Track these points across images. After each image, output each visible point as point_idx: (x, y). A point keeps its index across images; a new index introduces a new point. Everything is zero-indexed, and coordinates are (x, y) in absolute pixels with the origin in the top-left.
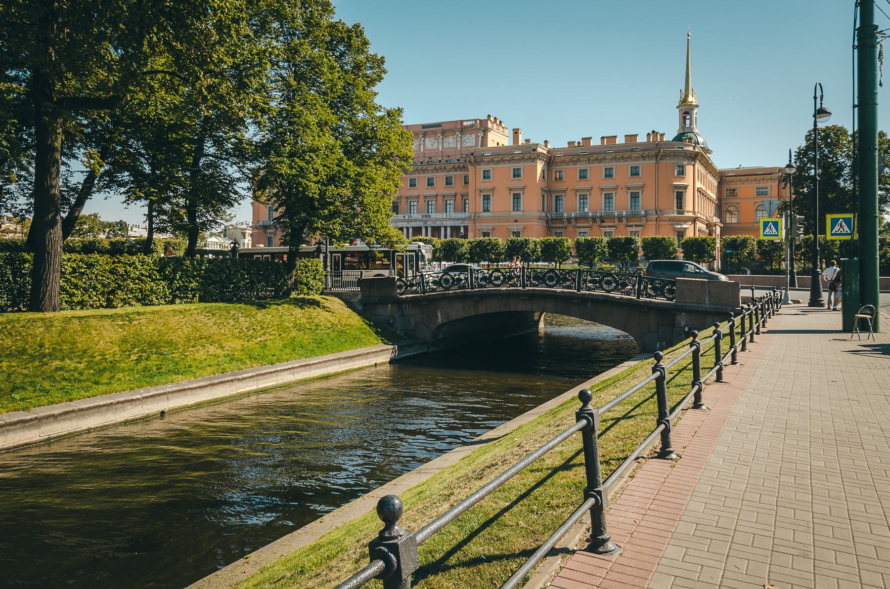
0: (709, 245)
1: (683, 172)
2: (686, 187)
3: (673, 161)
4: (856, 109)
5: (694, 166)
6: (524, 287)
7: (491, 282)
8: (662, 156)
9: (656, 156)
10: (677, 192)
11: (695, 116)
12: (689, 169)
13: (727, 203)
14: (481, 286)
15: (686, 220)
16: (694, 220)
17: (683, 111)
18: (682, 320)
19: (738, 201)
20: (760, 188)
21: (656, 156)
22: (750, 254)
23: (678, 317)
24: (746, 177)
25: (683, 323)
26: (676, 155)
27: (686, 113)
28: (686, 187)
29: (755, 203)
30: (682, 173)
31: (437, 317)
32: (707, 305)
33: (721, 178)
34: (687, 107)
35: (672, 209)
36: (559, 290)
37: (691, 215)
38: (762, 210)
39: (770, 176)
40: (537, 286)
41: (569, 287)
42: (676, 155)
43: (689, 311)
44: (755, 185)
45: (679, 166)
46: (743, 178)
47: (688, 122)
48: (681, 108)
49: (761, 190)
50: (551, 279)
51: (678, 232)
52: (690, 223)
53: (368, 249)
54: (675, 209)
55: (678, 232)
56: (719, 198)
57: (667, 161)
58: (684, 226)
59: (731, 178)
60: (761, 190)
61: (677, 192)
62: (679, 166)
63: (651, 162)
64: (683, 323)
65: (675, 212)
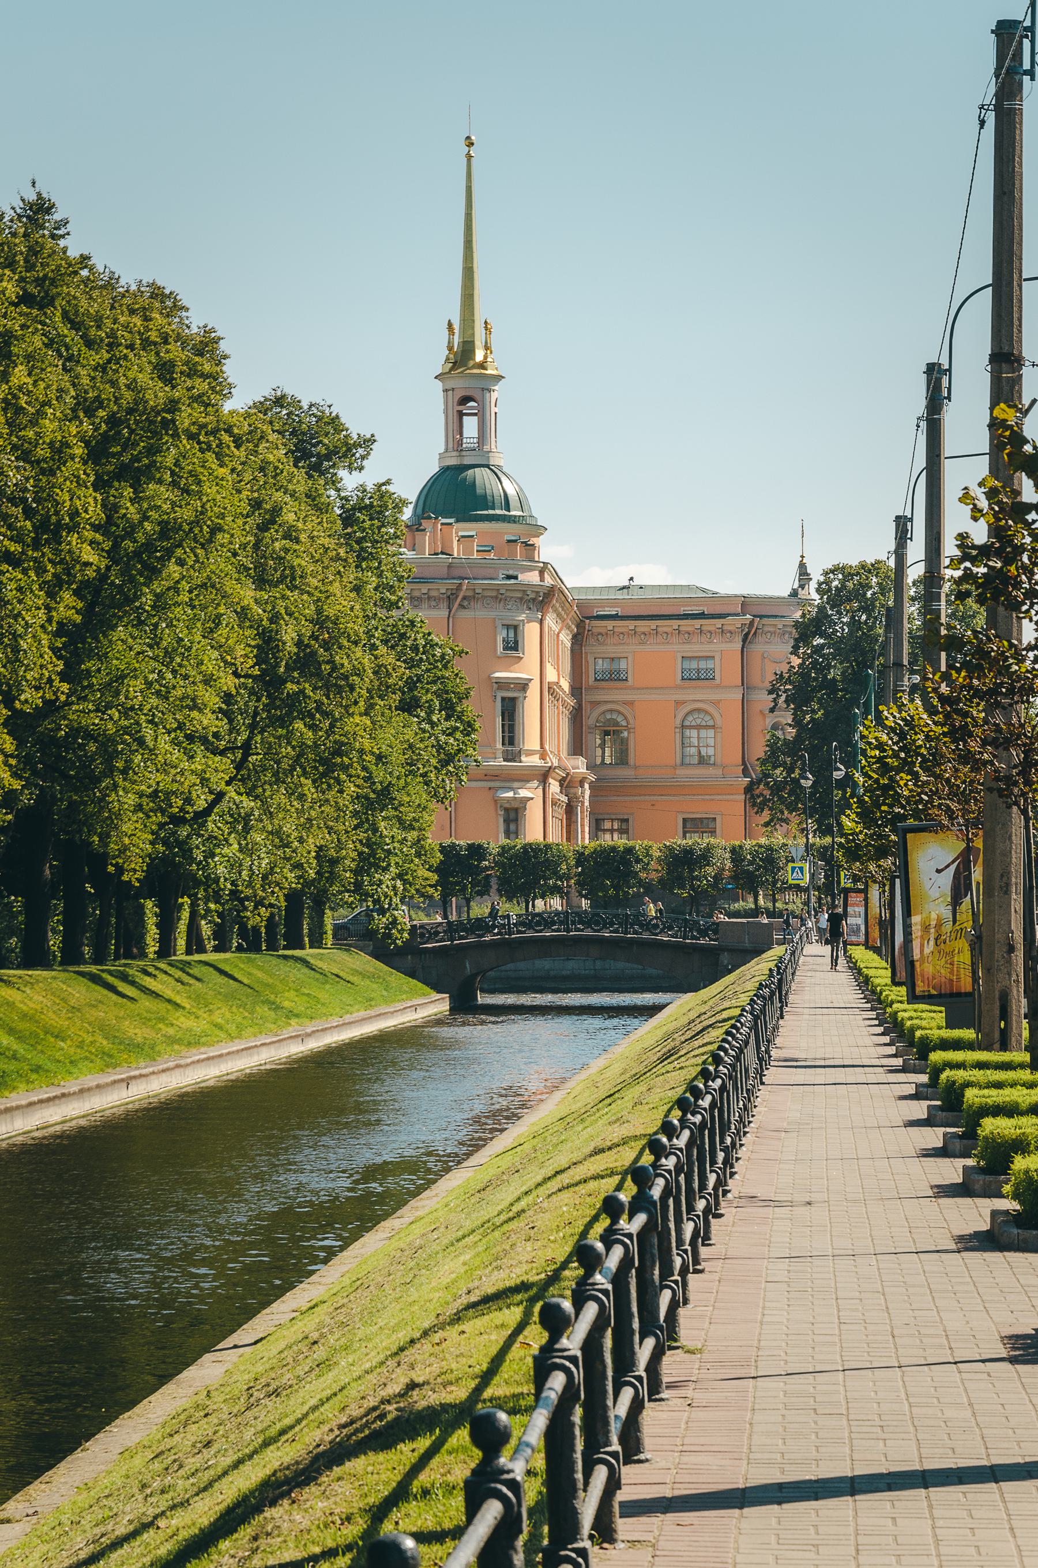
0: (638, 861)
1: (516, 642)
2: (523, 686)
3: (492, 614)
4: (1026, 65)
5: (541, 622)
6: (510, 935)
7: (648, 930)
8: (464, 598)
9: (450, 598)
10: (503, 699)
11: (494, 409)
12: (531, 632)
13: (599, 703)
14: (519, 932)
15: (524, 777)
16: (544, 776)
17: (459, 394)
18: (725, 959)
19: (629, 698)
20: (691, 658)
21: (450, 598)
22: (717, 877)
23: (721, 957)
24: (653, 624)
25: (726, 962)
26: (499, 597)
27: (465, 400)
28: (523, 686)
29: (679, 703)
30: (513, 645)
31: (465, 967)
32: (747, 945)
33: (580, 625)
34: (473, 383)
35: (491, 744)
36: (430, 946)
37: (535, 761)
38: (698, 727)
39: (718, 623)
40: (582, 931)
41: (616, 931)
42: (499, 597)
43: (731, 950)
44: (678, 648)
45: (508, 627)
46: (643, 626)
47: (471, 426)
48: (451, 384)
49: (694, 665)
50: (538, 924)
51: (507, 810)
52: (535, 784)
53: (135, 872)
54: (499, 745)
55: (507, 810)
56: (576, 690)
57: (479, 614)
58: (523, 793)
59: (610, 624)
60: (694, 665)
61: (503, 699)
62: (508, 627)
63: (434, 613)
64: (726, 962)
65: (499, 754)
